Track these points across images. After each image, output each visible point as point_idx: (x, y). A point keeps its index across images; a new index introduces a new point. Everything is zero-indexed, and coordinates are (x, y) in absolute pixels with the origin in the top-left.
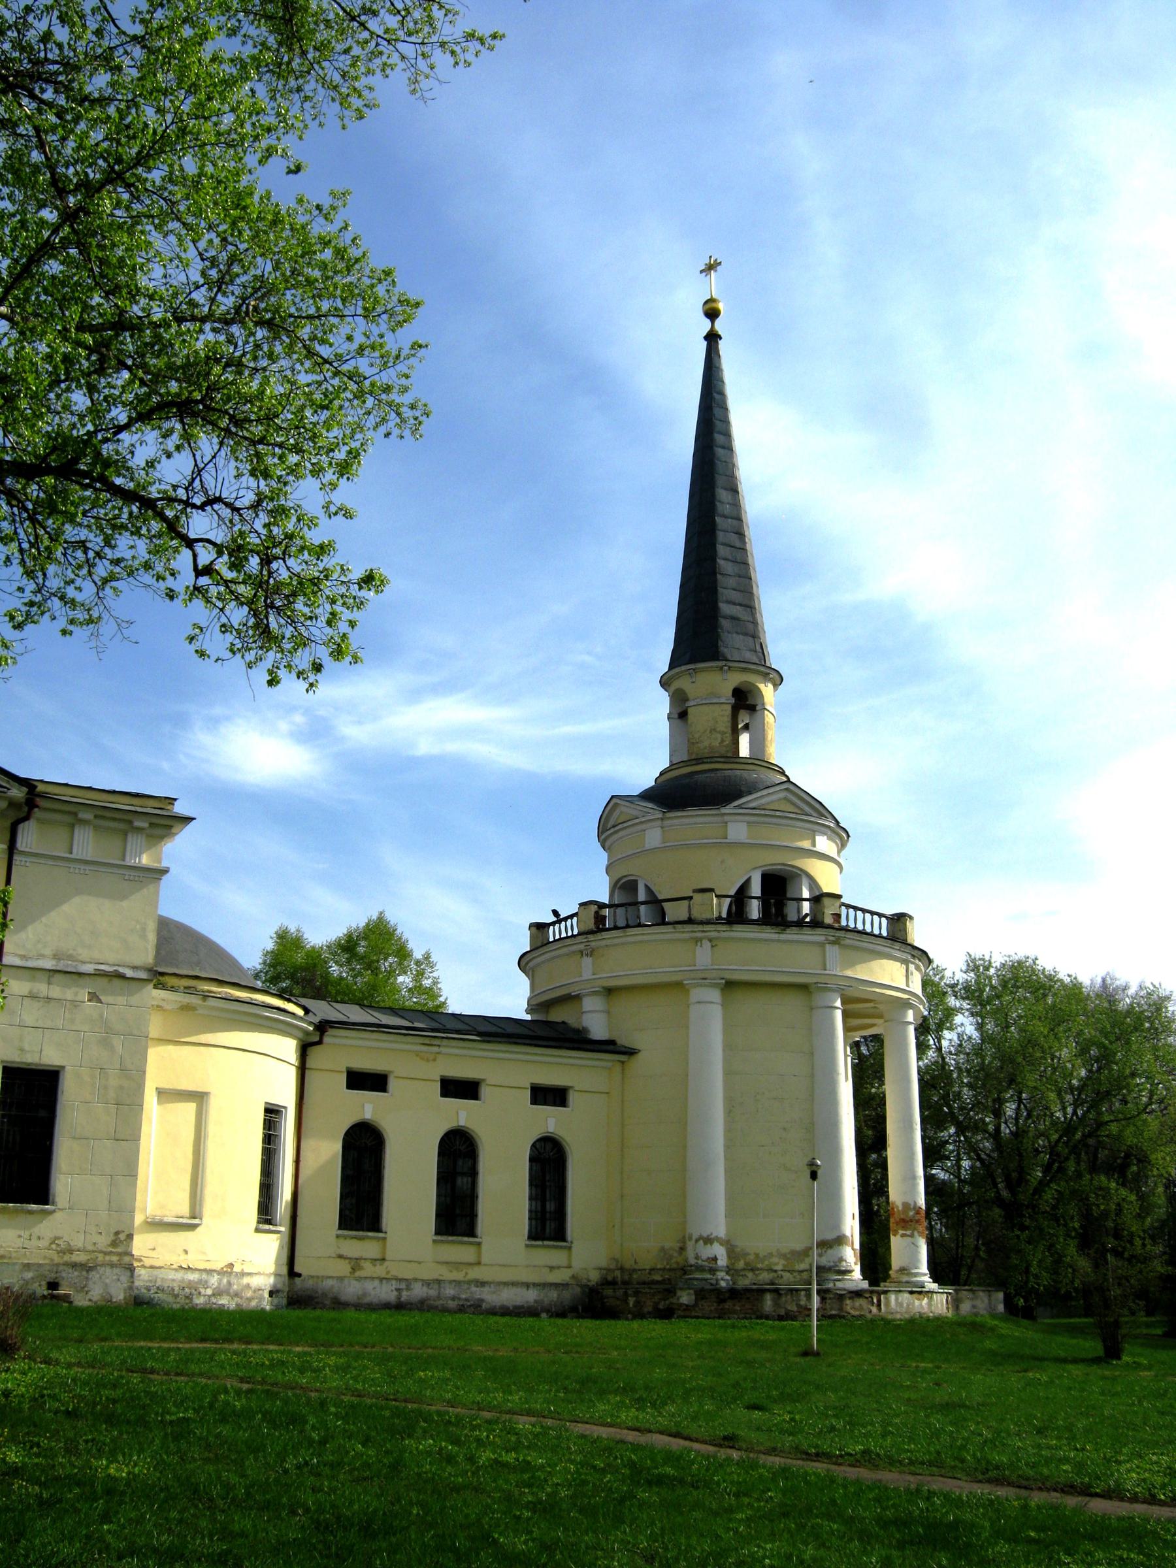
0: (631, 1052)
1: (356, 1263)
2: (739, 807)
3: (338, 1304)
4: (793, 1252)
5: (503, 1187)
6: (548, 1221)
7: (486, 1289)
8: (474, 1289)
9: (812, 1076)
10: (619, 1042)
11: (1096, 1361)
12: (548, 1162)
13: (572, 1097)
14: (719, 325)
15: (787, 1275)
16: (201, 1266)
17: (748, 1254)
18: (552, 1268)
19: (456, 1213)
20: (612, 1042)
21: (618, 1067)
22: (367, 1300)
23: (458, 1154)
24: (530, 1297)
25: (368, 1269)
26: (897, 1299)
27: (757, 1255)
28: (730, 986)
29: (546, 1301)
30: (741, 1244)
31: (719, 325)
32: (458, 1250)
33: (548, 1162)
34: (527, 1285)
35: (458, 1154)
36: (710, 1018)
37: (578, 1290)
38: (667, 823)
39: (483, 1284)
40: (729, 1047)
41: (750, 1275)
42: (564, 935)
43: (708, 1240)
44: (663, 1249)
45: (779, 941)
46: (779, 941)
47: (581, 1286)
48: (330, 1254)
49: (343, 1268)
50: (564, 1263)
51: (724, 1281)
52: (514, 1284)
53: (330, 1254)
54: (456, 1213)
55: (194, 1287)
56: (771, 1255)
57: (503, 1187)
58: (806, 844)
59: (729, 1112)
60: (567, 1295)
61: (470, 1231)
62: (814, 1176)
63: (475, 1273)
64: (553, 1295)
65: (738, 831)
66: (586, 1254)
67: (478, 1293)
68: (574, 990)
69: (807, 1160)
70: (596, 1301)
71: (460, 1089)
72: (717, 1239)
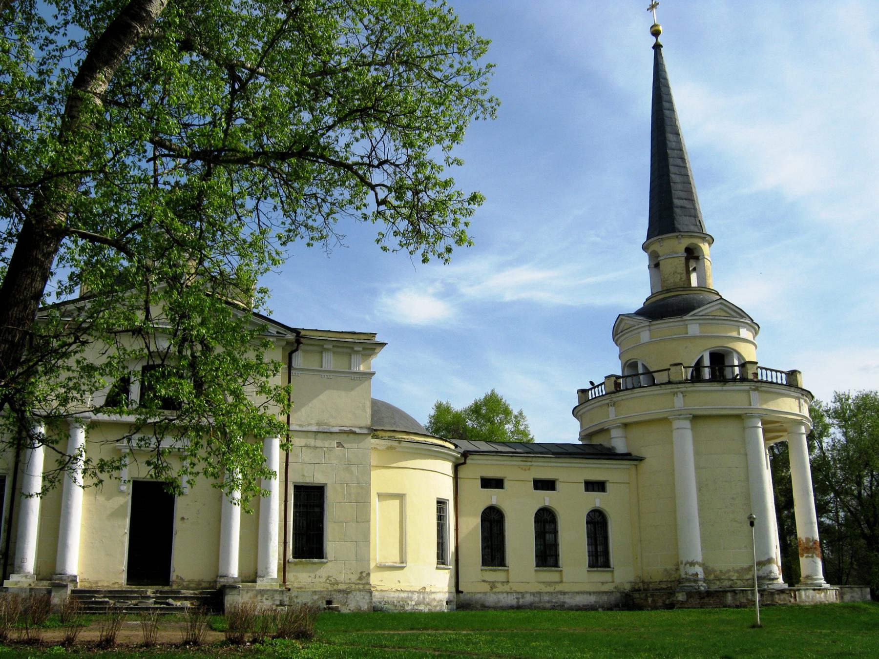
0: (640, 459)
1: (493, 585)
2: (694, 315)
3: (484, 607)
4: (742, 569)
5: (573, 539)
6: (599, 557)
7: (567, 596)
8: (560, 596)
12: (597, 524)
13: (609, 486)
14: (661, 40)
15: (739, 582)
18: (603, 583)
19: (547, 554)
20: (629, 454)
21: (633, 468)
22: (500, 605)
23: (546, 521)
24: (592, 599)
25: (500, 588)
27: (721, 571)
28: (695, 418)
30: (711, 565)
31: (661, 40)
32: (549, 575)
33: (597, 524)
34: (590, 593)
35: (546, 521)
36: (685, 438)
37: (619, 595)
39: (564, 593)
40: (697, 454)
41: (718, 583)
43: (692, 564)
44: (666, 570)
45: (722, 391)
46: (722, 391)
48: (478, 580)
49: (486, 587)
53: (478, 580)
54: (547, 554)
55: (405, 601)
56: (729, 571)
57: (573, 539)
58: (734, 334)
59: (700, 490)
60: (613, 599)
61: (606, 564)
63: (559, 587)
64: (605, 598)
65: (694, 329)
66: (622, 574)
67: (562, 598)
70: (629, 601)
72: (697, 563)
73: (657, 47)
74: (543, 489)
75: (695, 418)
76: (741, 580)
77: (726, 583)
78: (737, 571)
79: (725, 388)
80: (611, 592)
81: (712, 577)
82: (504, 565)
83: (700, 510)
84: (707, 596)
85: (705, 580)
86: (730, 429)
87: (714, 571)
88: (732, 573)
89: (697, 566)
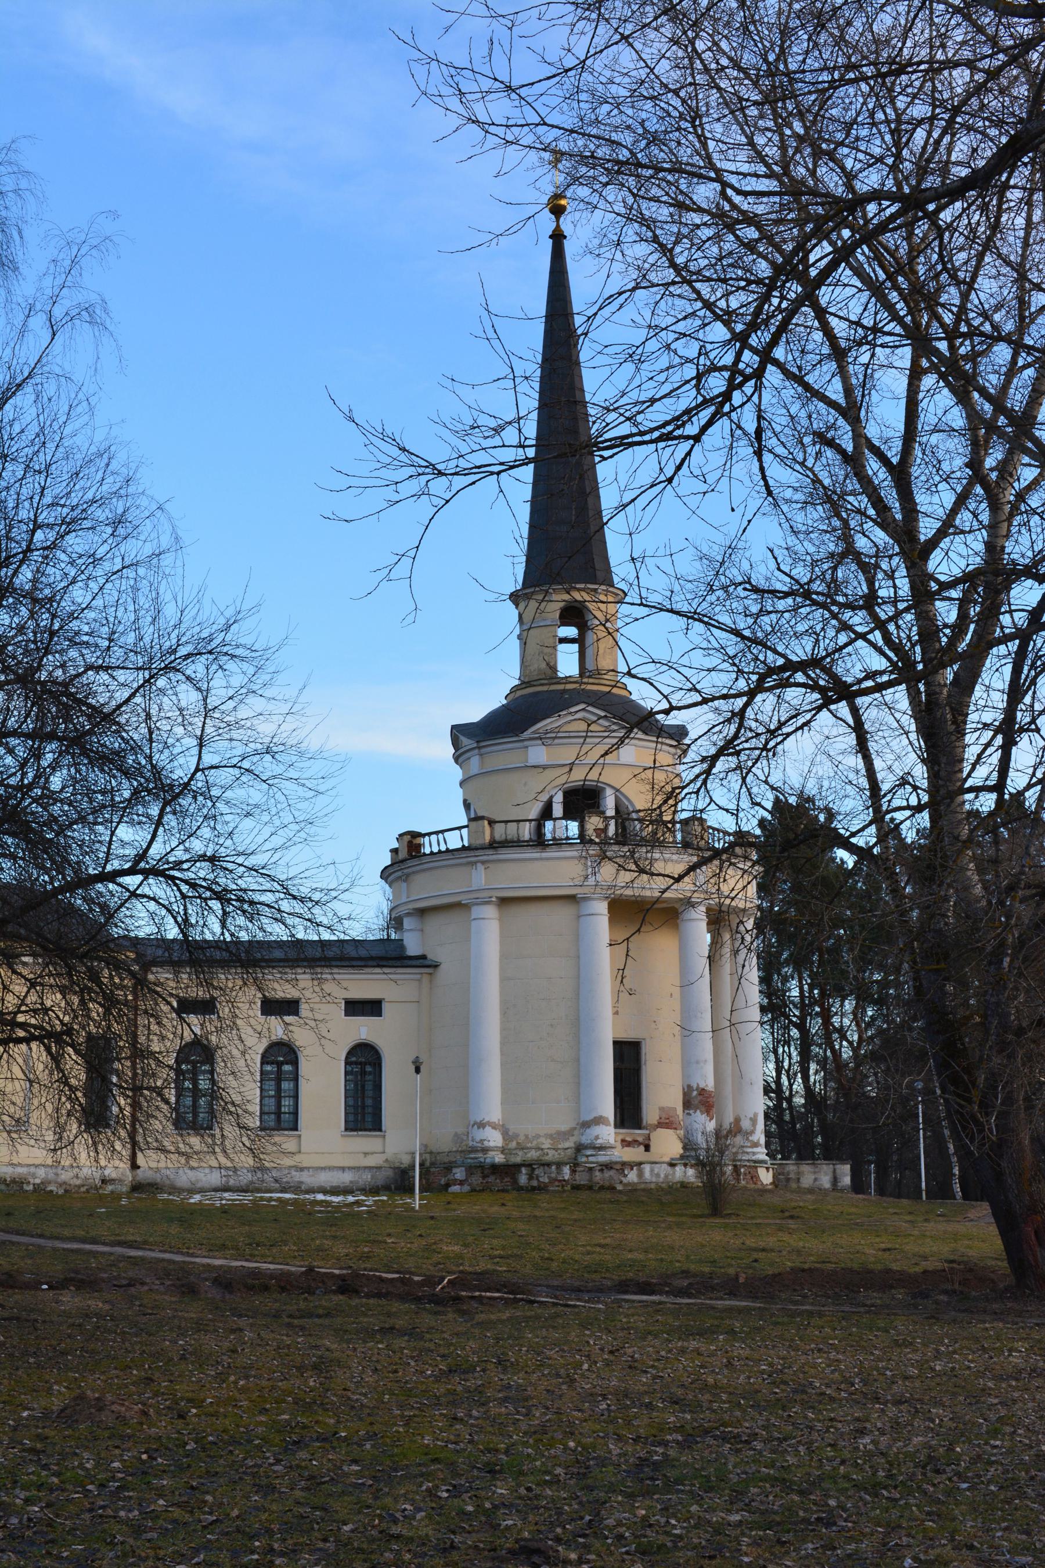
0: (436, 966)
2: (534, 732)
4: (559, 1133)
5: (323, 1086)
6: (364, 1112)
7: (305, 1173)
8: (294, 1173)
9: (578, 977)
10: (429, 956)
11: (708, 1216)
13: (386, 1007)
15: (551, 1153)
16: (30, 1161)
17: (517, 1136)
18: (366, 1154)
20: (424, 957)
21: (425, 979)
22: (199, 1185)
24: (346, 1178)
26: (652, 1171)
27: (527, 1136)
28: (504, 902)
29: (361, 1183)
30: (513, 1128)
33: (364, 1063)
34: (343, 1169)
36: (489, 928)
37: (390, 1173)
38: (483, 750)
39: (302, 1169)
41: (520, 1153)
42: (435, 850)
43: (481, 1125)
44: (456, 1135)
45: (541, 859)
46: (541, 859)
47: (395, 1168)
50: (380, 1149)
51: (499, 1158)
52: (330, 1168)
56: (538, 1136)
57: (323, 1086)
59: (504, 1013)
60: (381, 1178)
61: (376, 1126)
62: (418, 1070)
64: (367, 1177)
65: (538, 754)
66: (400, 1141)
67: (297, 1177)
68: (464, 899)
69: (412, 1058)
71: (371, 1008)
72: (489, 1124)
73: (558, 237)
74: (363, 1015)
75: (504, 902)
76: (556, 1150)
77: (533, 1155)
78: (550, 1136)
79: (544, 855)
80: (379, 1168)
81: (513, 1145)
82: (380, 1130)
83: (504, 1042)
84: (493, 1173)
85: (503, 1150)
86: (562, 914)
87: (516, 1136)
88: (542, 1140)
89: (488, 1129)
